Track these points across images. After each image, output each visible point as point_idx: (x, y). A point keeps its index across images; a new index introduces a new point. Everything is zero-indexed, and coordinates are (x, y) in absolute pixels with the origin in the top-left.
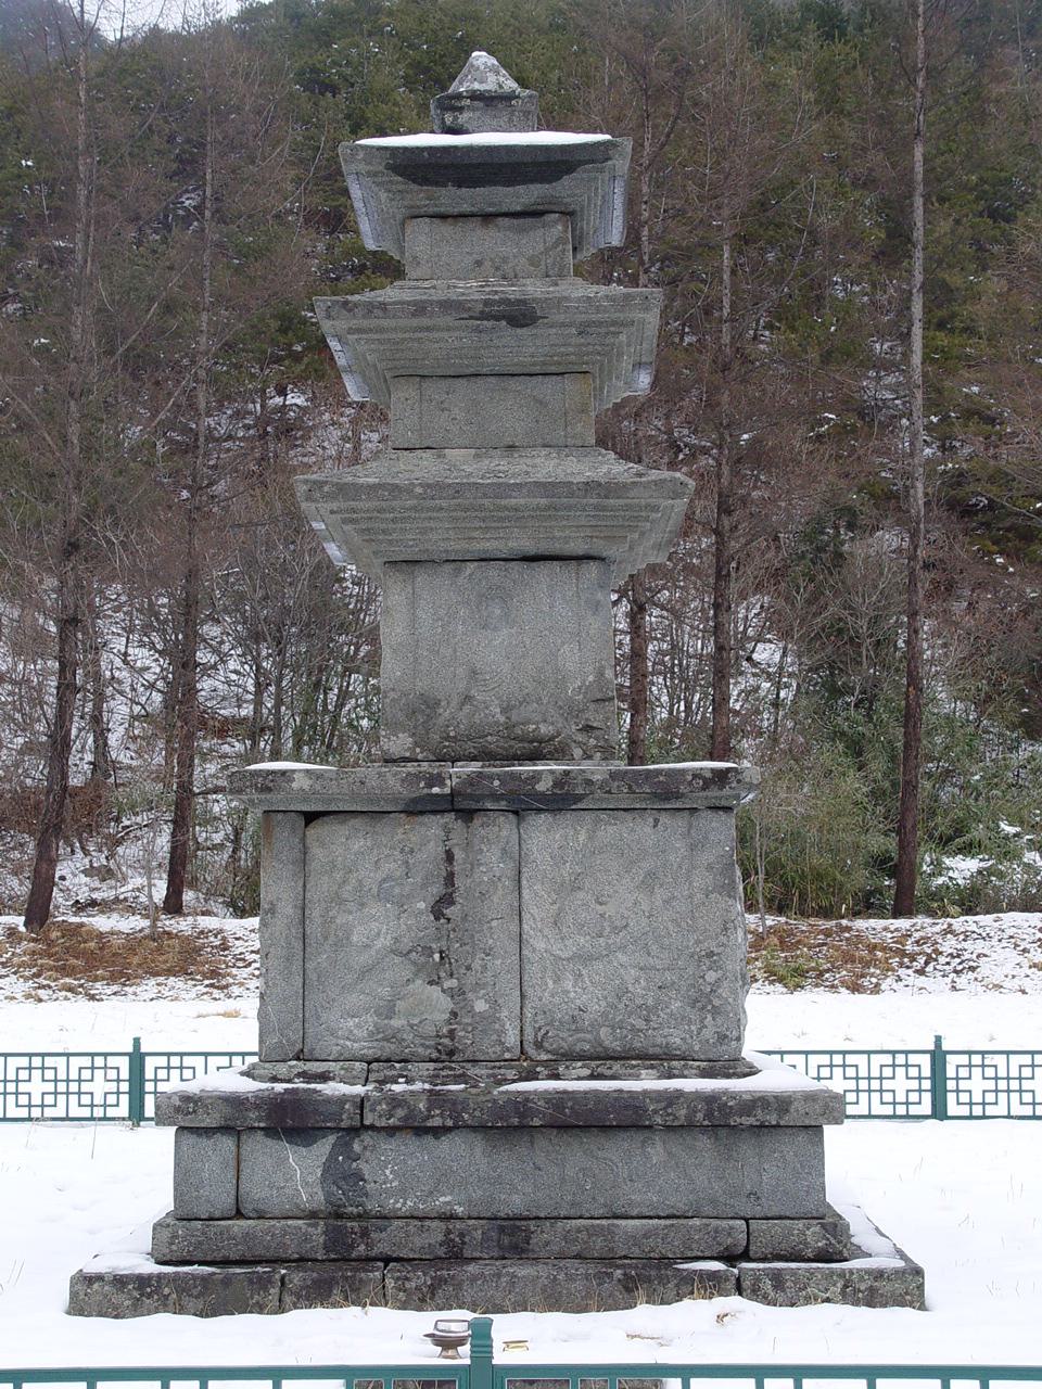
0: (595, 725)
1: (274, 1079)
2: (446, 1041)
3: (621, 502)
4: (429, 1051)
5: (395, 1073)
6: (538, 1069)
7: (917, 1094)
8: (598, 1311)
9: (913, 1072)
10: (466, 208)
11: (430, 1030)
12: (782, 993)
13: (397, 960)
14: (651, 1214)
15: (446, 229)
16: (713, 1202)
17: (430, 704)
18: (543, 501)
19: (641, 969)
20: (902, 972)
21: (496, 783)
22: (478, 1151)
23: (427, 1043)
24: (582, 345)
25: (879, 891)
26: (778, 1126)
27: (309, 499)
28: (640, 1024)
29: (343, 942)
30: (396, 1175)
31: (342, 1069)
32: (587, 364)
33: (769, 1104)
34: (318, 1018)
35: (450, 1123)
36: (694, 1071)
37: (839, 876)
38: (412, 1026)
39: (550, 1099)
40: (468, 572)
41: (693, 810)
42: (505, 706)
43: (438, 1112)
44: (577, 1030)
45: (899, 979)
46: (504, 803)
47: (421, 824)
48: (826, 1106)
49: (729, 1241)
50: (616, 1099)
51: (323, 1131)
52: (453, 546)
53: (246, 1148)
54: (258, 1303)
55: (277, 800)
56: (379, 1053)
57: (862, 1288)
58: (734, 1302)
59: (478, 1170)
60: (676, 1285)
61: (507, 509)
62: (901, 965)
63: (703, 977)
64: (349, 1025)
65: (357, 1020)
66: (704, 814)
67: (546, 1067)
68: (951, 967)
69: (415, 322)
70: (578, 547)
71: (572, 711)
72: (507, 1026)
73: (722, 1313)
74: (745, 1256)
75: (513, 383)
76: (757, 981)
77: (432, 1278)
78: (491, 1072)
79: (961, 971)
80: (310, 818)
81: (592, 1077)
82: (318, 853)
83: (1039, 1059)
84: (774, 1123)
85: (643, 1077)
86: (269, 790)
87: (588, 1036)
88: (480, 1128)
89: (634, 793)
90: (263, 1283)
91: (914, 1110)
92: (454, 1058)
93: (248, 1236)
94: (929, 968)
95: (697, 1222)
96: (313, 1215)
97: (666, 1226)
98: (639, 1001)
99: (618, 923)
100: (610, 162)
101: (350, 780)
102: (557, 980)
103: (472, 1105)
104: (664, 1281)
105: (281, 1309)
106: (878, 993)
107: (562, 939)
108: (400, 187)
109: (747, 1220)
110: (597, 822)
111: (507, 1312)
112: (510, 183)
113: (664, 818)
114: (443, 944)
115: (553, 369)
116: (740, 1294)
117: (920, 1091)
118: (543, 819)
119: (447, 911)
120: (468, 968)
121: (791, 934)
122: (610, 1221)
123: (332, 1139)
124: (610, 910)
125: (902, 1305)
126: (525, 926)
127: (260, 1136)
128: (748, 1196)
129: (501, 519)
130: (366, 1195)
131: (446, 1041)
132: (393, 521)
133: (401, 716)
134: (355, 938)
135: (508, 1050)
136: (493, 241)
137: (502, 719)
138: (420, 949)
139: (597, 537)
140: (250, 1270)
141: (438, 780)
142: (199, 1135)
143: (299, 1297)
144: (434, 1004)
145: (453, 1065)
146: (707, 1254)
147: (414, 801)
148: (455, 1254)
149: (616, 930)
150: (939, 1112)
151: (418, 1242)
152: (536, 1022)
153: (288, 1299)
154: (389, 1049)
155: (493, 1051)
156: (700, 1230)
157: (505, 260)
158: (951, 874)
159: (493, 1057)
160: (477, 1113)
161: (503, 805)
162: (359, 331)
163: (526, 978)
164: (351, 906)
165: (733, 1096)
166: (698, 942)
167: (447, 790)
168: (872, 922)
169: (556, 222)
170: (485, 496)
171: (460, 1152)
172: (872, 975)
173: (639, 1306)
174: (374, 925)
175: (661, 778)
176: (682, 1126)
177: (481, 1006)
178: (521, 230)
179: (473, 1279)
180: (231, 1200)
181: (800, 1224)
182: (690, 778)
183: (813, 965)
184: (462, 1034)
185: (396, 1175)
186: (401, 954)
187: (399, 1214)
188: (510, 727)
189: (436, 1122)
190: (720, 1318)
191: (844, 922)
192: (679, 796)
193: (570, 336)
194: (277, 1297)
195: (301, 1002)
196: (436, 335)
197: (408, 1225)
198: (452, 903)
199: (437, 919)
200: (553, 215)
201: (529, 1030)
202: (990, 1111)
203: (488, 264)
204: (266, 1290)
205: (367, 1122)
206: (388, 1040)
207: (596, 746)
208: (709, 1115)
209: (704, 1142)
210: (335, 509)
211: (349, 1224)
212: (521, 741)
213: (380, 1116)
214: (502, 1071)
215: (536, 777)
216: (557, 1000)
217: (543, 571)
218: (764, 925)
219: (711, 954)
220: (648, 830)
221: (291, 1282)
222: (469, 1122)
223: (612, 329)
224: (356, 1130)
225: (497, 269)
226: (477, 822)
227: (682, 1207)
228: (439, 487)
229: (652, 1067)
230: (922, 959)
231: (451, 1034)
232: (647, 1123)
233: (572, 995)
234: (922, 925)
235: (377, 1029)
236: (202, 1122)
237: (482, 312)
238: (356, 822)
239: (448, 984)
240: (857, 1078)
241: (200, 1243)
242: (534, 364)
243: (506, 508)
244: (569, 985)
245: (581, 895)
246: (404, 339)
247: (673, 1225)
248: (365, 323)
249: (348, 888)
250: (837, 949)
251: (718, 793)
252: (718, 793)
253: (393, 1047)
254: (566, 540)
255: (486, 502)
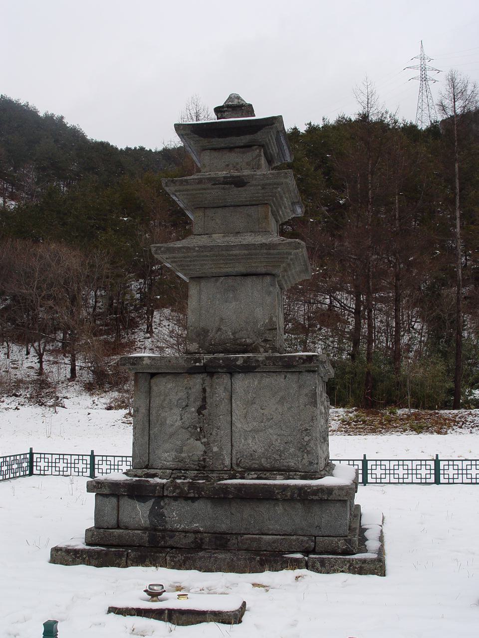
0: (269, 339)
1: (136, 476)
2: (202, 463)
3: (275, 251)
4: (196, 466)
5: (181, 474)
6: (237, 475)
7: (427, 477)
8: (249, 573)
9: (428, 467)
10: (223, 145)
11: (196, 458)
12: (415, 434)
13: (184, 430)
14: (277, 533)
15: (216, 154)
16: (302, 529)
17: (205, 331)
18: (246, 252)
19: (278, 435)
20: (454, 427)
21: (221, 361)
22: (209, 506)
23: (195, 463)
24: (264, 193)
25: (449, 401)
26: (327, 500)
27: (156, 253)
28: (277, 457)
29: (163, 424)
30: (178, 515)
31: (162, 472)
32: (266, 200)
33: (324, 491)
34: (154, 452)
35: (197, 496)
36: (298, 477)
37: (435, 396)
38: (189, 456)
39: (236, 487)
40: (221, 280)
41: (300, 372)
42: (233, 331)
43: (192, 491)
44: (253, 459)
45: (453, 430)
46: (225, 369)
47: (194, 378)
48: (347, 492)
49: (307, 545)
50: (262, 488)
51: (150, 498)
52: (214, 270)
53: (121, 502)
54: (118, 563)
55: (139, 368)
56: (177, 466)
57: (357, 567)
58: (304, 571)
59: (208, 514)
60: (281, 564)
61: (233, 256)
62: (454, 425)
63: (303, 439)
64: (166, 456)
65: (168, 454)
66: (304, 374)
67: (240, 474)
68: (470, 426)
69: (199, 186)
70: (263, 270)
71: (259, 334)
72: (226, 457)
73: (298, 575)
74: (314, 552)
75: (239, 209)
76: (407, 430)
77: (184, 557)
78: (218, 475)
79: (474, 427)
80: (153, 375)
81: (258, 478)
82: (155, 388)
83: (478, 463)
84: (326, 498)
85: (278, 478)
86: (135, 364)
87: (257, 462)
88: (208, 498)
89: (275, 365)
90: (119, 555)
91: (428, 481)
92: (206, 469)
93: (120, 536)
94: (463, 426)
95: (294, 537)
96: (145, 529)
97: (282, 539)
98: (278, 448)
99: (269, 417)
100: (274, 125)
101: (165, 360)
102: (246, 439)
103: (205, 489)
104: (276, 562)
105: (126, 566)
106: (446, 434)
107: (248, 423)
108: (197, 139)
109: (315, 537)
110: (262, 377)
111: (213, 572)
112: (238, 135)
113: (288, 375)
114: (201, 424)
115: (254, 203)
116: (307, 569)
117: (430, 474)
118: (240, 376)
119: (203, 412)
120: (211, 434)
121: (419, 415)
122: (260, 536)
123: (153, 500)
124: (266, 412)
125: (373, 573)
126: (233, 418)
127: (126, 498)
128: (316, 528)
129: (231, 260)
130: (166, 522)
131: (202, 463)
132: (190, 261)
133: (194, 337)
134: (168, 422)
135: (226, 467)
136: (233, 158)
137: (232, 337)
138: (192, 426)
139: (269, 266)
140: (117, 550)
141: (199, 360)
142: (104, 497)
143: (133, 561)
144: (198, 448)
145: (204, 472)
146: (298, 550)
147: (191, 368)
148: (198, 546)
149: (268, 420)
150: (437, 482)
151: (184, 541)
152: (237, 456)
153: (129, 562)
154: (181, 465)
155: (220, 467)
156: (295, 541)
157: (237, 164)
158: (475, 395)
159: (220, 469)
160: (207, 492)
161: (225, 370)
162: (179, 191)
163: (233, 438)
164: (167, 409)
165: (309, 487)
166: (301, 425)
167: (202, 364)
168: (446, 411)
169: (256, 149)
170: (222, 250)
171: (202, 507)
172: (444, 428)
173: (266, 572)
174: (175, 417)
175: (286, 359)
176: (289, 499)
177: (215, 449)
178: (243, 153)
179: (200, 558)
180: (115, 522)
181: (336, 539)
182: (297, 359)
183: (426, 425)
184: (208, 460)
185: (178, 515)
186: (185, 429)
187: (179, 530)
188: (235, 340)
189: (192, 495)
190: (297, 578)
191: (437, 411)
192: (294, 366)
193: (259, 189)
194: (125, 561)
195: (148, 446)
196: (209, 191)
197: (180, 535)
198: (205, 408)
199: (199, 415)
200: (255, 147)
201: (234, 459)
202: (456, 481)
203: (231, 165)
204: (121, 559)
205: (165, 494)
206: (180, 462)
207: (269, 348)
208: (299, 495)
209: (299, 506)
210: (168, 257)
211: (158, 533)
212: (240, 345)
213: (170, 492)
214: (223, 475)
215: (237, 359)
216: (245, 447)
217: (249, 281)
218: (410, 412)
219: (307, 430)
220: (282, 380)
221: (130, 555)
222: (204, 496)
223: (275, 186)
224: (163, 497)
225: (235, 167)
226: (215, 377)
227: (289, 531)
228: (205, 247)
229: (282, 475)
230: (461, 423)
231: (204, 460)
232: (275, 498)
233: (251, 445)
234: (463, 412)
235: (176, 457)
236: (104, 491)
237: (223, 181)
238: (169, 377)
239: (203, 440)
240: (394, 474)
241: (103, 538)
242: (247, 201)
243: (232, 255)
244: (250, 441)
245: (255, 406)
246: (197, 193)
247: (284, 539)
248: (181, 188)
249: (166, 402)
250: (434, 420)
251: (309, 365)
252: (309, 365)
253: (182, 464)
254: (257, 267)
255: (224, 252)
